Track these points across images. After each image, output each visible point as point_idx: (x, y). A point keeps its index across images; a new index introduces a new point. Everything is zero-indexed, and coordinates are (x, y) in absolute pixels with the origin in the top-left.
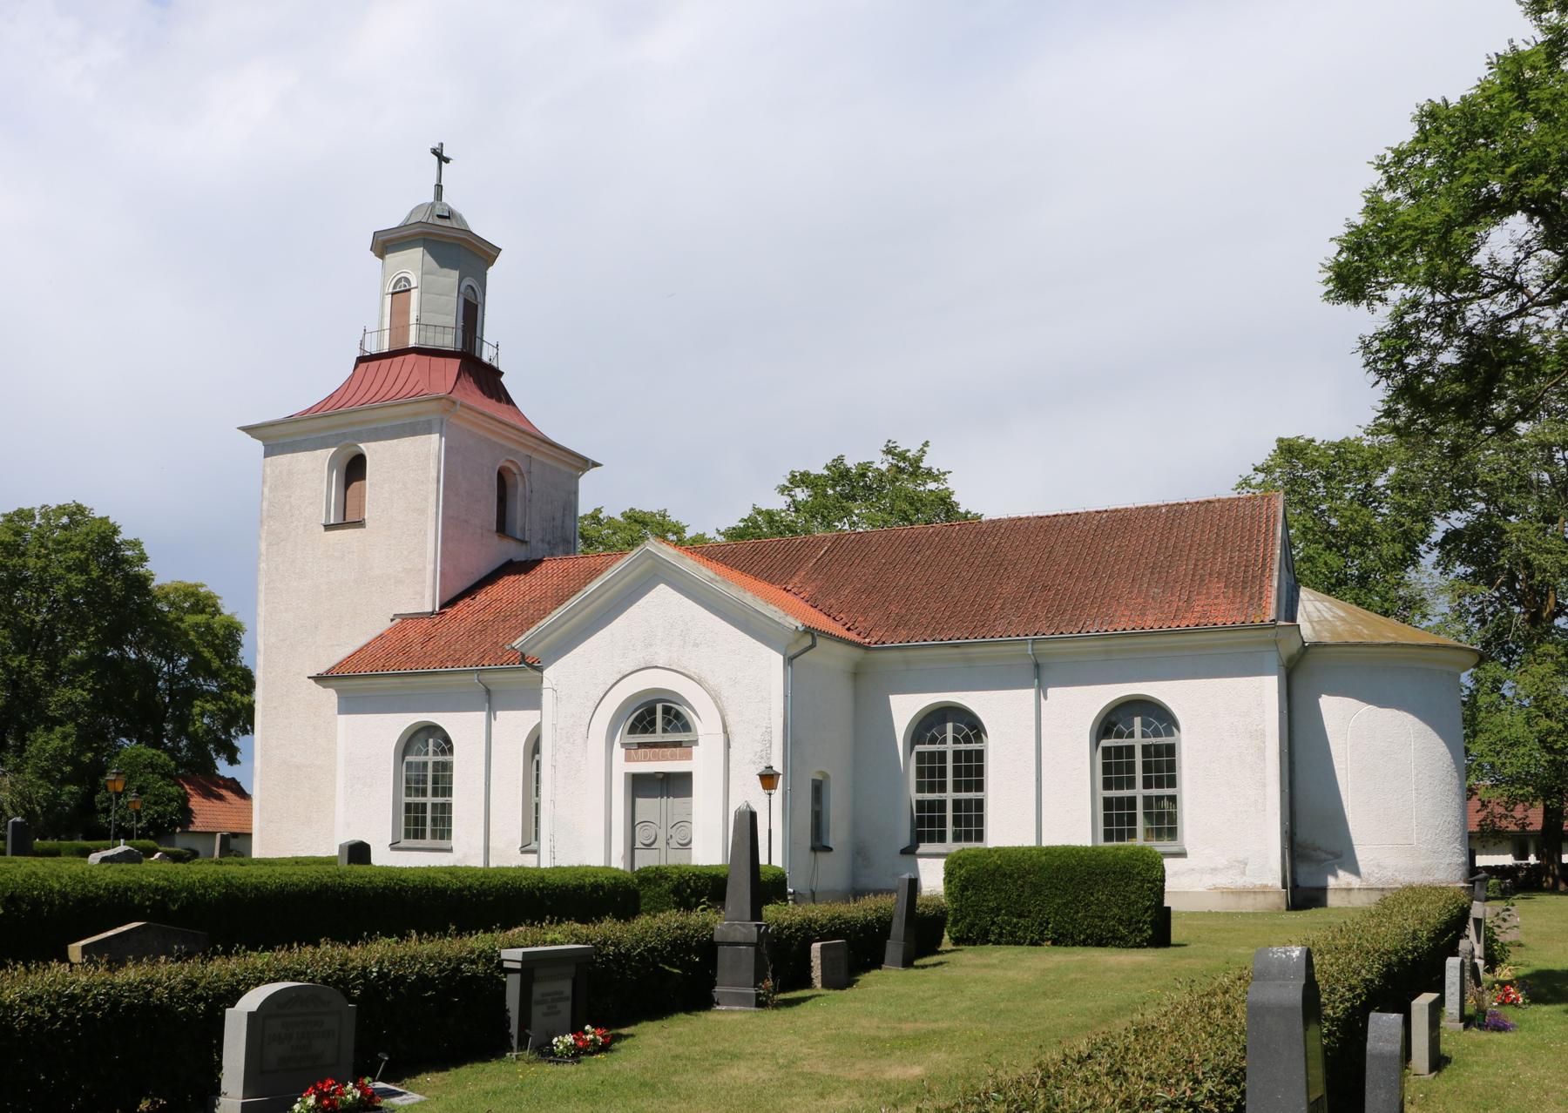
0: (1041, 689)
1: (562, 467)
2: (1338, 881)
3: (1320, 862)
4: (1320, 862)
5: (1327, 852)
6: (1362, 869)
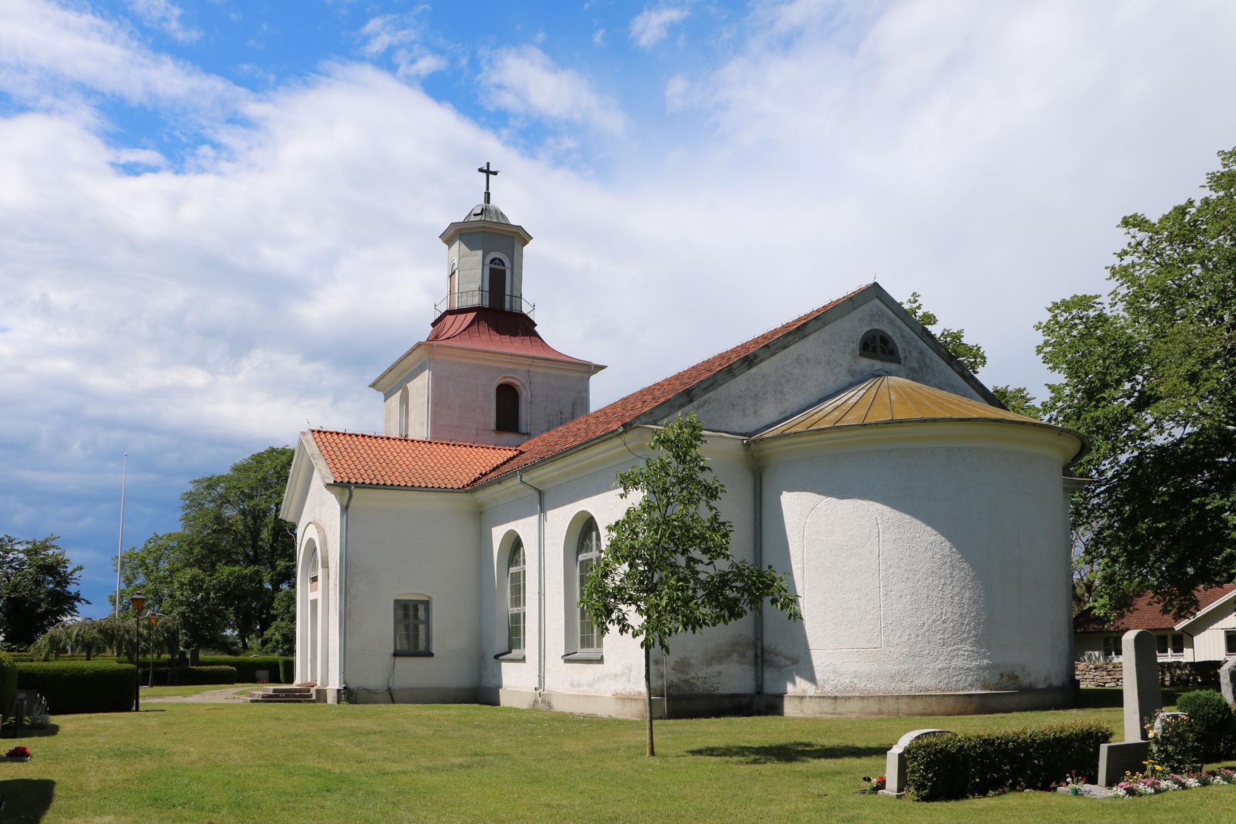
0: (543, 511)
1: (570, 374)
2: (797, 687)
3: (781, 667)
4: (781, 667)
5: (786, 658)
6: (819, 676)
